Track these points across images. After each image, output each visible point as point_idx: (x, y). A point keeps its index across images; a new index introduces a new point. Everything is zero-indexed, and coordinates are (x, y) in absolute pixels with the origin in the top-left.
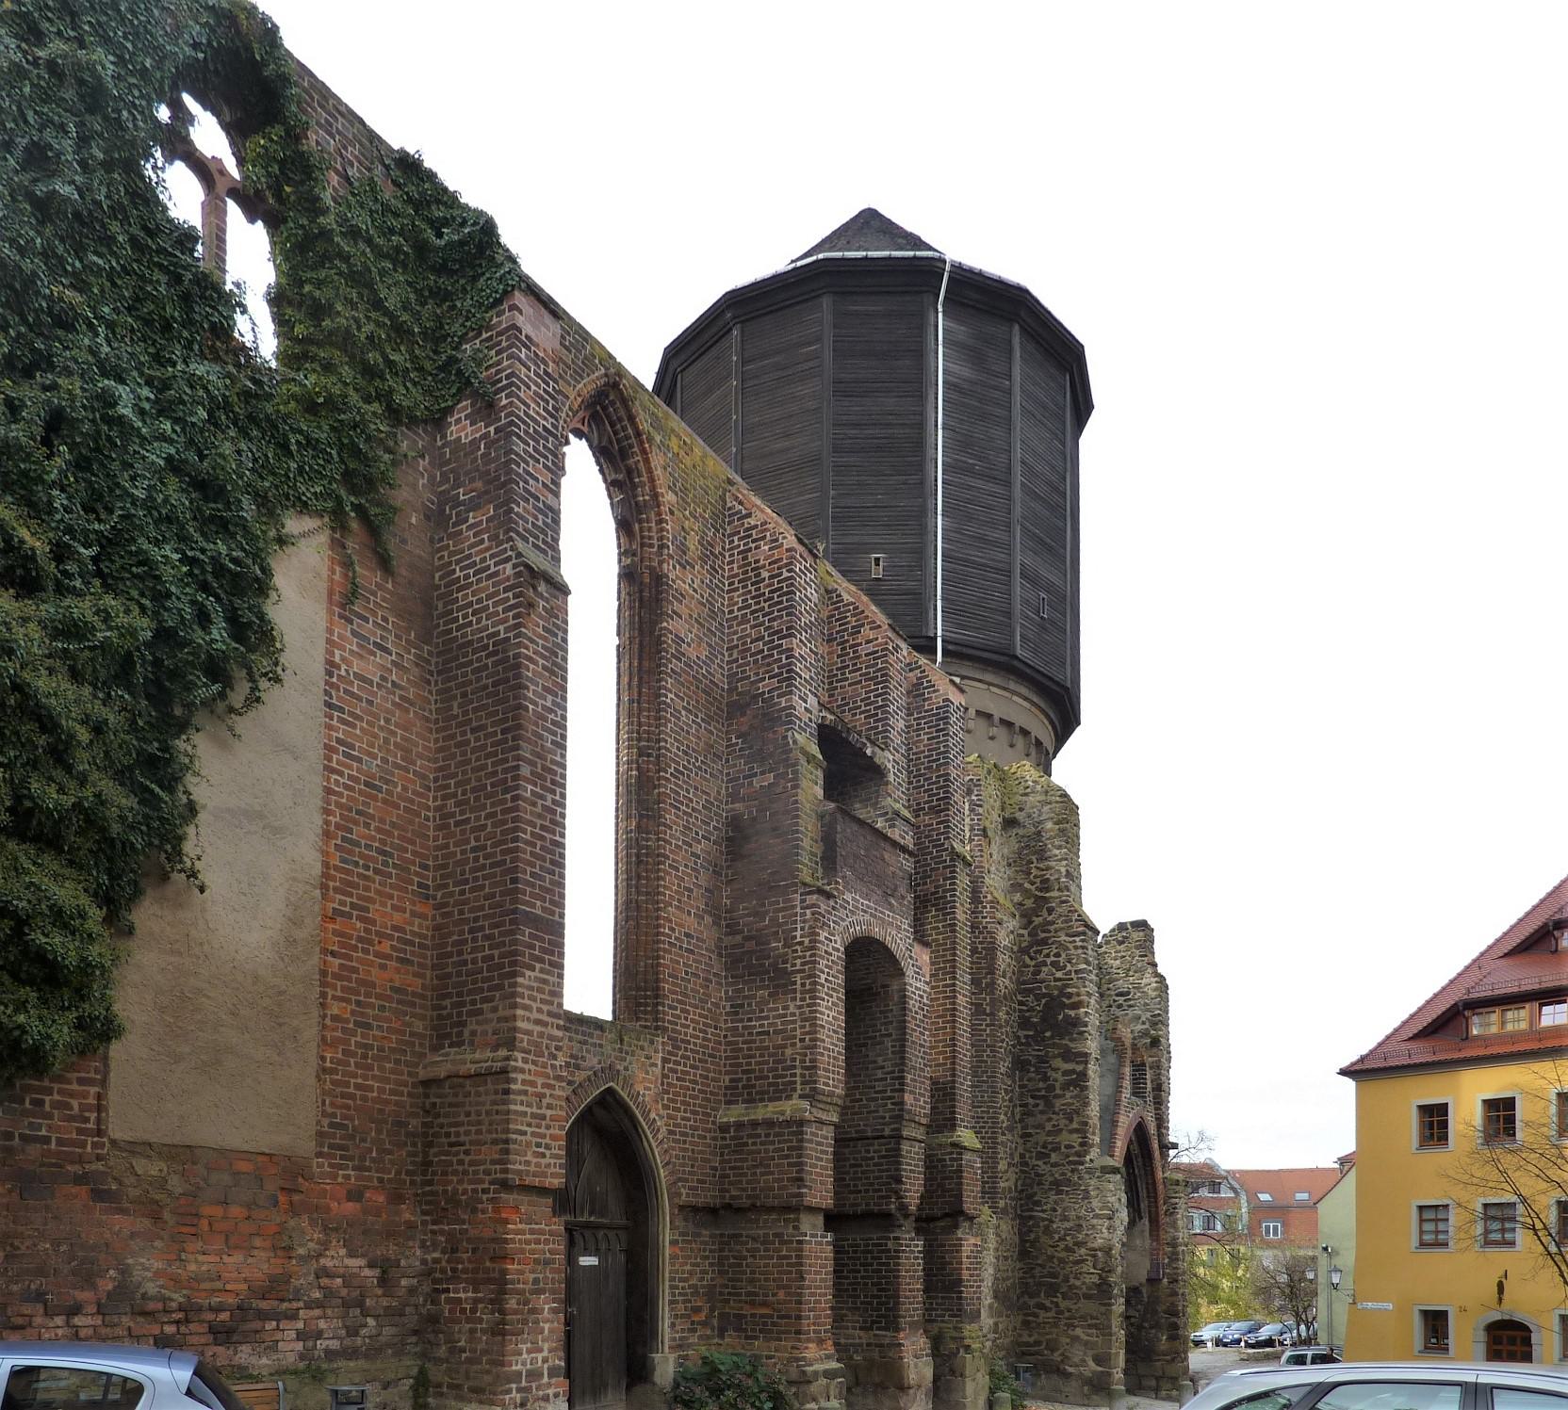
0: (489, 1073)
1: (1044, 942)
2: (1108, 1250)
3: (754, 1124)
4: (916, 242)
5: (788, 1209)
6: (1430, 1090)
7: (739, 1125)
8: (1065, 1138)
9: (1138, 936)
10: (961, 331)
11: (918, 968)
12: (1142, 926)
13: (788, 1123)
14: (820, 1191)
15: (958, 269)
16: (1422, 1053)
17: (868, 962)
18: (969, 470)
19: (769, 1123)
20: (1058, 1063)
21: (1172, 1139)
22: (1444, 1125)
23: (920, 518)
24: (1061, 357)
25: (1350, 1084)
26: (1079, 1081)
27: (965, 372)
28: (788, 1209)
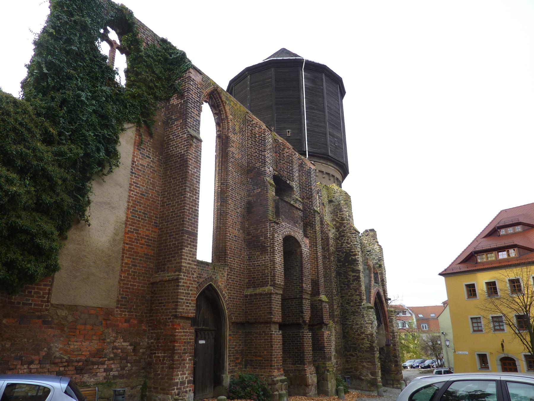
0: (173, 280)
1: (343, 236)
2: (372, 335)
3: (256, 295)
5: (267, 323)
6: (469, 279)
9: (371, 233)
10: (309, 75)
13: (266, 294)
14: (277, 317)
16: (463, 268)
18: (313, 109)
19: (261, 294)
20: (351, 273)
21: (389, 297)
24: (336, 82)
25: (442, 278)
27: (311, 85)
28: (267, 323)
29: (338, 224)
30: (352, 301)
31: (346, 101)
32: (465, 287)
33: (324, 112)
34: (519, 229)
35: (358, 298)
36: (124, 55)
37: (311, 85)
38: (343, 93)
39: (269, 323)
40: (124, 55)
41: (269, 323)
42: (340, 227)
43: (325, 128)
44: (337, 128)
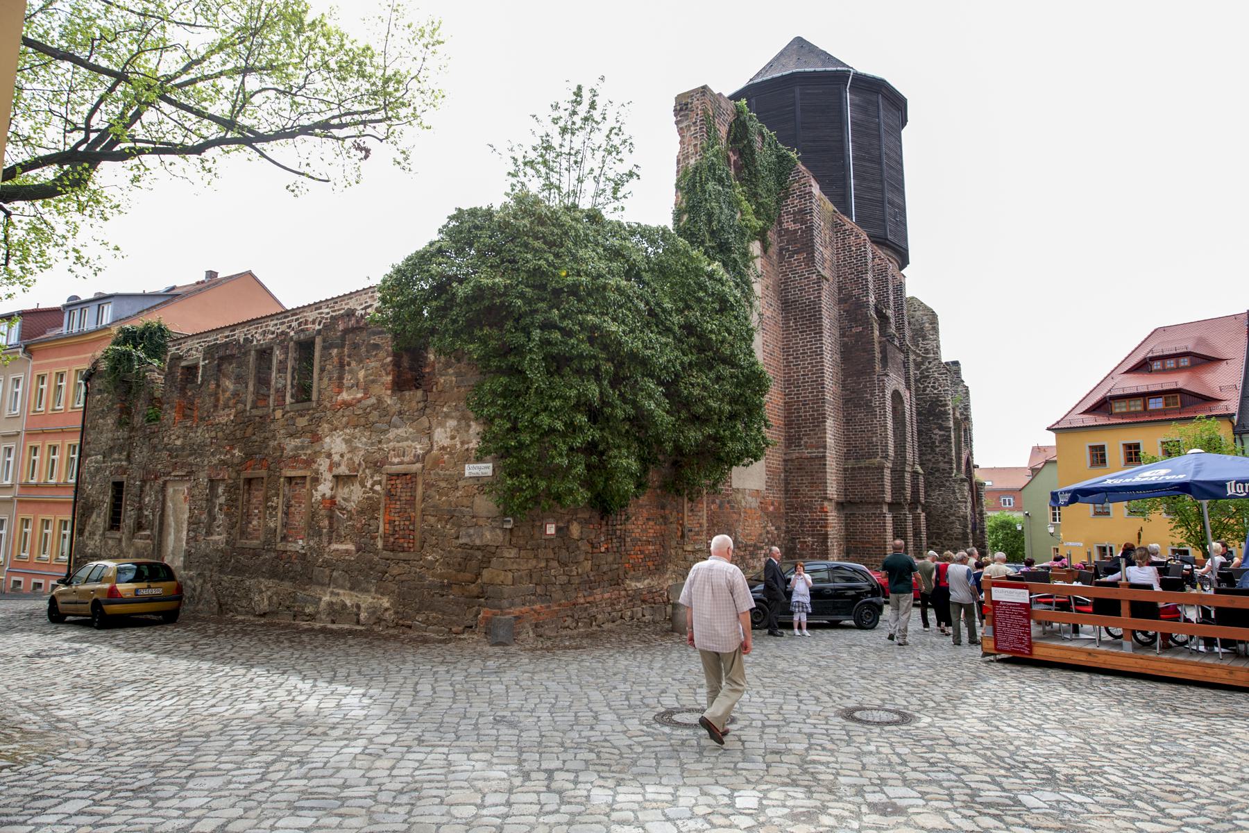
0: (817, 457)
1: (928, 377)
2: (965, 518)
3: (860, 468)
4: (844, 65)
5: (877, 503)
6: (1097, 439)
7: (853, 469)
8: (942, 465)
9: (954, 368)
10: (857, 100)
11: (906, 395)
12: (956, 363)
13: (877, 468)
14: (888, 498)
15: (856, 74)
16: (1090, 420)
17: (896, 395)
18: (864, 159)
19: (867, 468)
20: (936, 431)
21: (975, 463)
22: (1103, 455)
23: (845, 178)
24: (897, 104)
25: (1052, 435)
26: (946, 439)
27: (860, 117)
28: (877, 503)
29: (919, 359)
30: (938, 470)
31: (908, 134)
32: (1088, 450)
33: (880, 164)
34: (1185, 362)
35: (947, 466)
36: (946, 357)
37: (860, 117)
38: (904, 122)
39: (879, 503)
40: (946, 357)
41: (879, 503)
42: (922, 363)
43: (882, 191)
44: (898, 189)
